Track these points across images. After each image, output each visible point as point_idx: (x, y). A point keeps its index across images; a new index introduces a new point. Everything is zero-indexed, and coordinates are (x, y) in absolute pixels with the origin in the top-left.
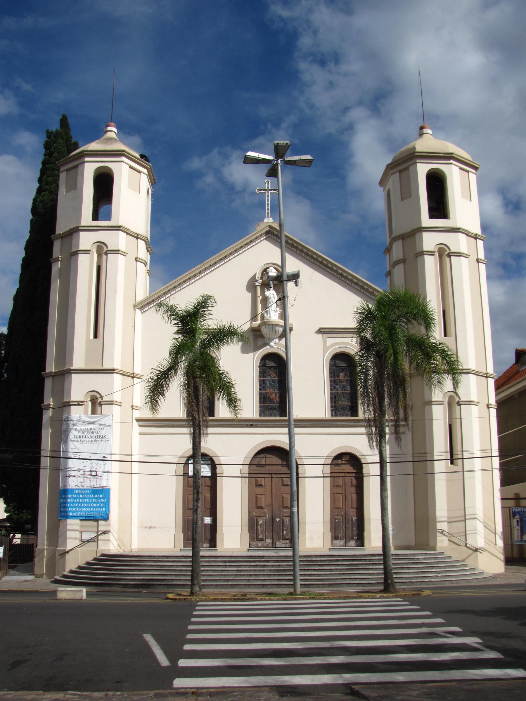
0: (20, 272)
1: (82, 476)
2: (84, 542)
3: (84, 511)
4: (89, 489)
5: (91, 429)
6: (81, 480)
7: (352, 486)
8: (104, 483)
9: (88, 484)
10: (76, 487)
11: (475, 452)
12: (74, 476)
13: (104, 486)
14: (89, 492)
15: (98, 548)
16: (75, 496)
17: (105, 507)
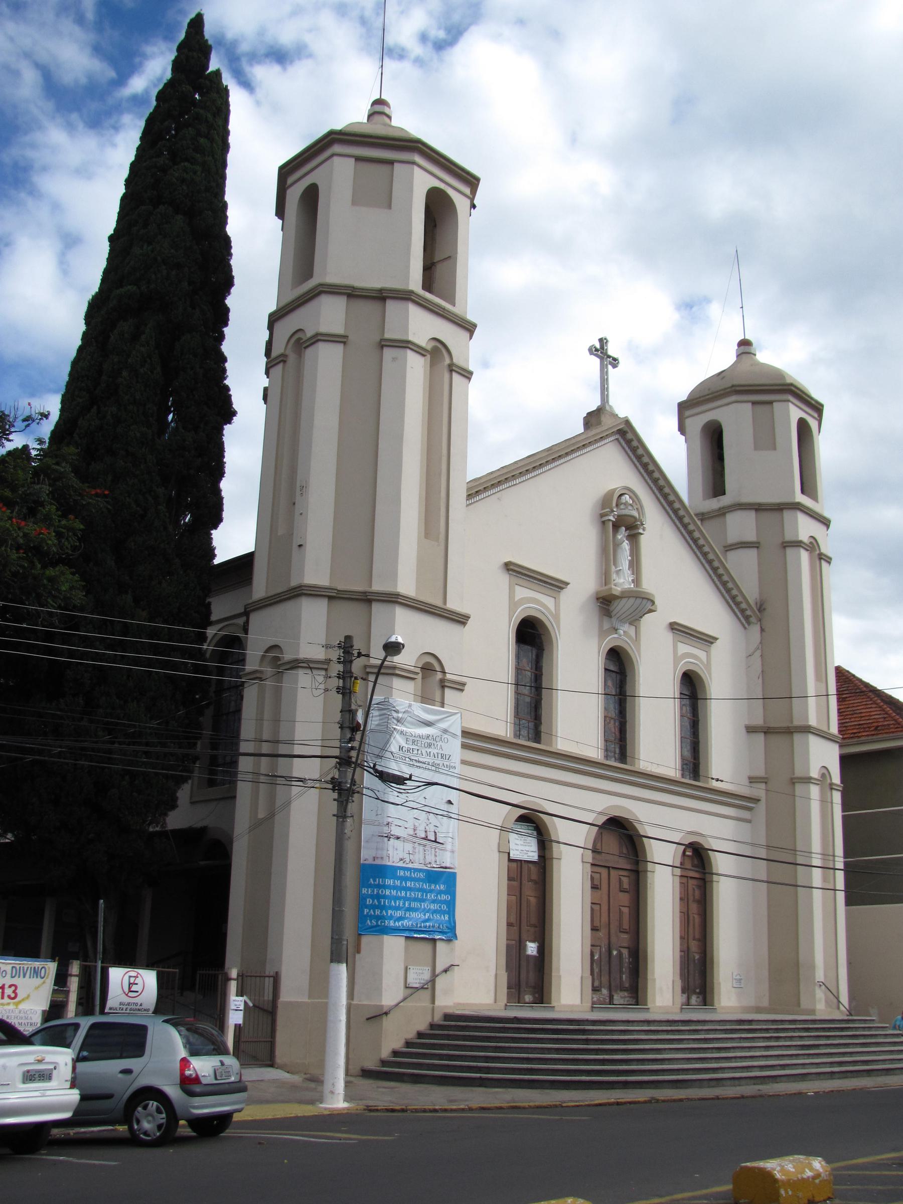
0: (95, 288)
1: (411, 838)
2: (411, 991)
3: (415, 918)
4: (420, 870)
5: (428, 737)
6: (409, 847)
7: (622, 890)
8: (447, 859)
9: (421, 858)
10: (401, 864)
11: (813, 855)
12: (398, 838)
13: (448, 865)
14: (422, 875)
15: (433, 1002)
16: (398, 883)
17: (448, 913)
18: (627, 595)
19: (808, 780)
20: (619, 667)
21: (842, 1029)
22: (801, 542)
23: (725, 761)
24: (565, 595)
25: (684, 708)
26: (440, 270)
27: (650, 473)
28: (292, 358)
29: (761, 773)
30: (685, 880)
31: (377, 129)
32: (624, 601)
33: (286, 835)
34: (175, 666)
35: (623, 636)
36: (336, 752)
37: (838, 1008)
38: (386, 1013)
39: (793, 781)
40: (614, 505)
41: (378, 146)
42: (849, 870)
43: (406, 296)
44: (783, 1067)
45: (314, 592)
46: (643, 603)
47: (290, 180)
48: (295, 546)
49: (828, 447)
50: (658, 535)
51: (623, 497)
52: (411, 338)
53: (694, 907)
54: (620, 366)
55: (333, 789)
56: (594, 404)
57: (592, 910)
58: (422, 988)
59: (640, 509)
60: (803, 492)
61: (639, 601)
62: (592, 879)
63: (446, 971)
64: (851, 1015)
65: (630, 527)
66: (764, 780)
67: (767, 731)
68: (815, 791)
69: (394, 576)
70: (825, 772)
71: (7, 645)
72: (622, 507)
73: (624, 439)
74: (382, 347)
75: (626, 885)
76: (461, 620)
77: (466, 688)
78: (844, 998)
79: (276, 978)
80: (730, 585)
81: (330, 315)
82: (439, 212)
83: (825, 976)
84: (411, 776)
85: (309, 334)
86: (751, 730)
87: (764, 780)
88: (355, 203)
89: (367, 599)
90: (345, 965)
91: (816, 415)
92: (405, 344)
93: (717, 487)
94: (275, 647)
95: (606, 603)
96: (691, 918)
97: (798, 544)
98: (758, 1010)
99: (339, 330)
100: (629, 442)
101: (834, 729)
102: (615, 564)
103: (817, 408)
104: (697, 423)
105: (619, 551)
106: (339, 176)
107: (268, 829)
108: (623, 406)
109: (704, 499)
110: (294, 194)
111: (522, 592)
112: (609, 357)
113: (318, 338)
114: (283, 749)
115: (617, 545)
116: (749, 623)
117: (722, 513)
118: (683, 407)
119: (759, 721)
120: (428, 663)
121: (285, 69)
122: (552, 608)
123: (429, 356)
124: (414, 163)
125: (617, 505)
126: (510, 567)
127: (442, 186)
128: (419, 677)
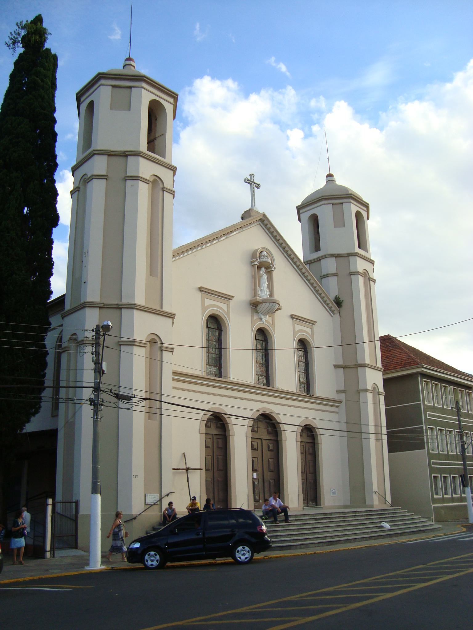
18: (265, 301)
19: (366, 391)
20: (263, 336)
21: (381, 514)
22: (359, 272)
23: (325, 382)
24: (232, 303)
25: (211, 351)
26: (157, 142)
27: (278, 241)
28: (82, 188)
29: (343, 388)
30: (303, 444)
31: (127, 71)
32: (264, 304)
33: (80, 429)
34: (10, 343)
35: (265, 322)
36: (93, 385)
37: (386, 503)
38: (135, 518)
39: (359, 392)
40: (258, 256)
41: (126, 80)
42: (389, 435)
43: (138, 154)
44: (344, 536)
45: (92, 305)
46: (273, 306)
47: (82, 100)
48: (83, 283)
49: (372, 225)
50: (283, 271)
51: (263, 254)
52: (140, 175)
53: (309, 457)
54: (261, 188)
55: (91, 404)
56: (248, 207)
57: (253, 461)
58: (154, 504)
59: (272, 259)
60: (359, 247)
61: (271, 304)
62: (252, 445)
63: (168, 495)
64: (392, 506)
65: (268, 268)
66: (344, 392)
67: (344, 367)
68: (370, 396)
69: (133, 296)
70: (375, 387)
71: (3, 343)
72: (262, 257)
73: (263, 224)
74: (126, 180)
75: (271, 448)
76: (171, 316)
77: (175, 351)
78: (389, 499)
79: (77, 503)
80: (323, 295)
81: (99, 165)
82: (155, 112)
83: (378, 489)
84: (134, 395)
85: (89, 175)
86: (336, 367)
87: (344, 392)
88: (111, 109)
89: (119, 307)
90: (99, 495)
91: (365, 209)
92: (137, 178)
93: (317, 247)
94: (75, 334)
95: (255, 305)
96: (307, 463)
97: (357, 273)
98: (346, 507)
99: (104, 173)
100: (266, 225)
101: (379, 365)
102: (259, 286)
103: (366, 206)
104: (306, 216)
105: (261, 280)
106: (103, 95)
107: (72, 426)
108: (260, 208)
109: (310, 253)
110: (84, 106)
111: (208, 302)
112: (255, 183)
113: (93, 177)
114: (78, 385)
115: (260, 277)
116: (334, 314)
117: (319, 260)
118: (299, 209)
119: (341, 362)
120: (153, 339)
121: (370, 128)
122: (226, 310)
123: (151, 184)
124: (142, 87)
125: (259, 257)
126: (201, 289)
127: (158, 99)
128: (148, 346)
